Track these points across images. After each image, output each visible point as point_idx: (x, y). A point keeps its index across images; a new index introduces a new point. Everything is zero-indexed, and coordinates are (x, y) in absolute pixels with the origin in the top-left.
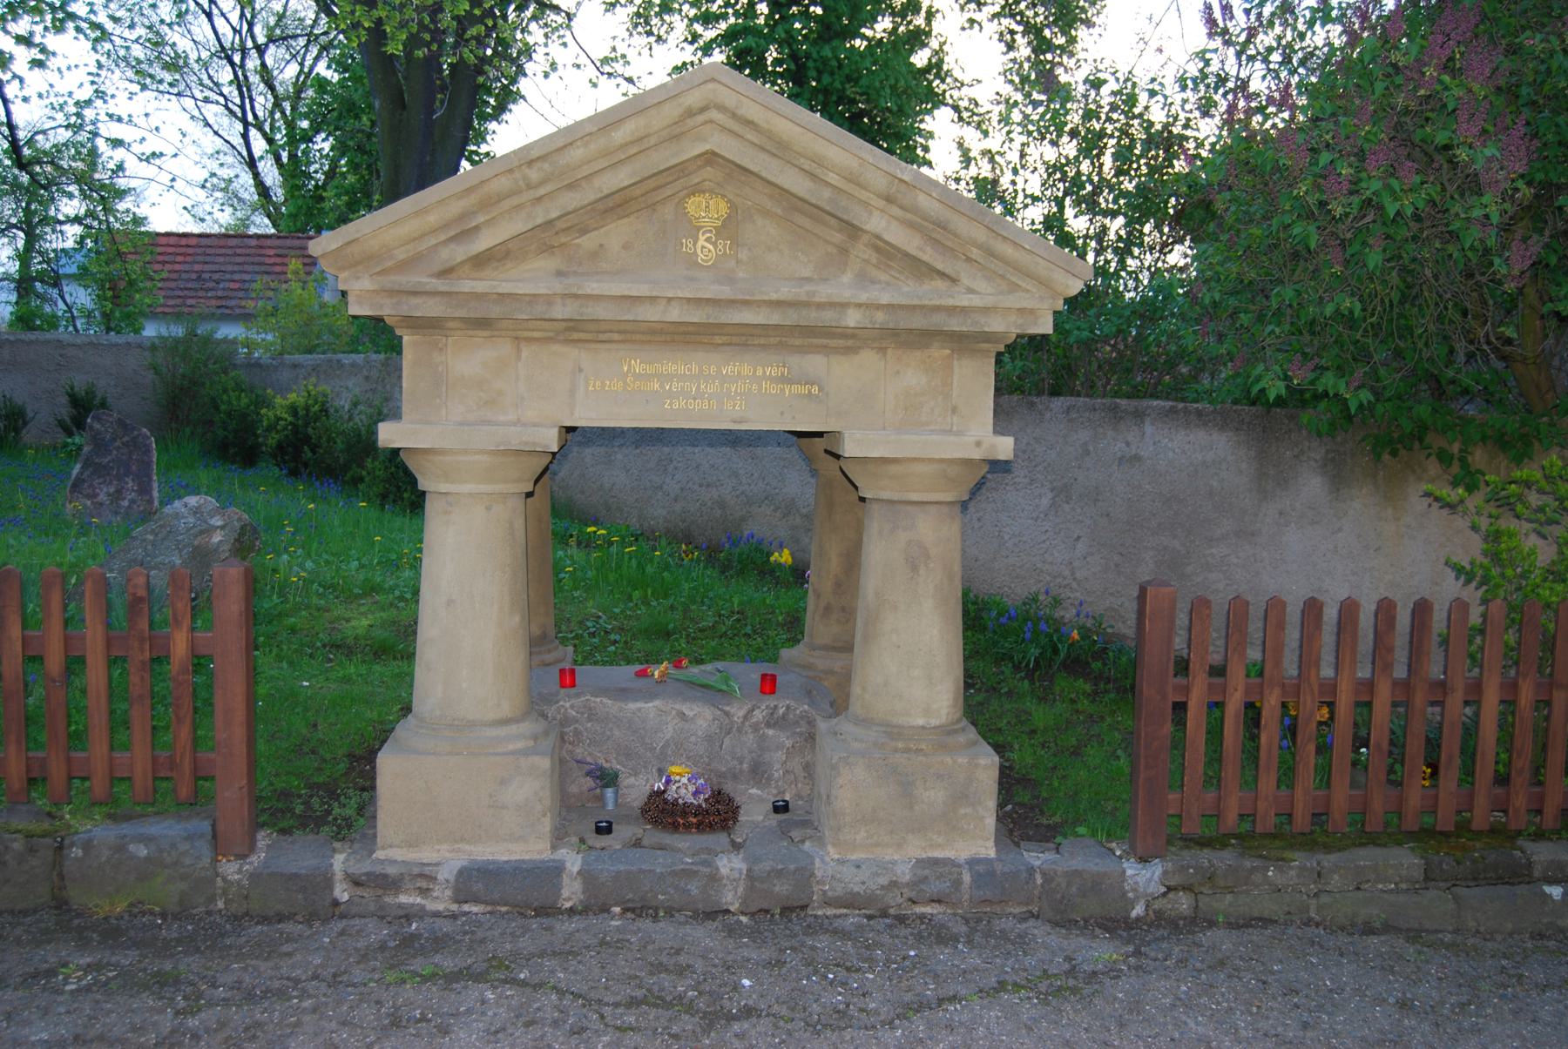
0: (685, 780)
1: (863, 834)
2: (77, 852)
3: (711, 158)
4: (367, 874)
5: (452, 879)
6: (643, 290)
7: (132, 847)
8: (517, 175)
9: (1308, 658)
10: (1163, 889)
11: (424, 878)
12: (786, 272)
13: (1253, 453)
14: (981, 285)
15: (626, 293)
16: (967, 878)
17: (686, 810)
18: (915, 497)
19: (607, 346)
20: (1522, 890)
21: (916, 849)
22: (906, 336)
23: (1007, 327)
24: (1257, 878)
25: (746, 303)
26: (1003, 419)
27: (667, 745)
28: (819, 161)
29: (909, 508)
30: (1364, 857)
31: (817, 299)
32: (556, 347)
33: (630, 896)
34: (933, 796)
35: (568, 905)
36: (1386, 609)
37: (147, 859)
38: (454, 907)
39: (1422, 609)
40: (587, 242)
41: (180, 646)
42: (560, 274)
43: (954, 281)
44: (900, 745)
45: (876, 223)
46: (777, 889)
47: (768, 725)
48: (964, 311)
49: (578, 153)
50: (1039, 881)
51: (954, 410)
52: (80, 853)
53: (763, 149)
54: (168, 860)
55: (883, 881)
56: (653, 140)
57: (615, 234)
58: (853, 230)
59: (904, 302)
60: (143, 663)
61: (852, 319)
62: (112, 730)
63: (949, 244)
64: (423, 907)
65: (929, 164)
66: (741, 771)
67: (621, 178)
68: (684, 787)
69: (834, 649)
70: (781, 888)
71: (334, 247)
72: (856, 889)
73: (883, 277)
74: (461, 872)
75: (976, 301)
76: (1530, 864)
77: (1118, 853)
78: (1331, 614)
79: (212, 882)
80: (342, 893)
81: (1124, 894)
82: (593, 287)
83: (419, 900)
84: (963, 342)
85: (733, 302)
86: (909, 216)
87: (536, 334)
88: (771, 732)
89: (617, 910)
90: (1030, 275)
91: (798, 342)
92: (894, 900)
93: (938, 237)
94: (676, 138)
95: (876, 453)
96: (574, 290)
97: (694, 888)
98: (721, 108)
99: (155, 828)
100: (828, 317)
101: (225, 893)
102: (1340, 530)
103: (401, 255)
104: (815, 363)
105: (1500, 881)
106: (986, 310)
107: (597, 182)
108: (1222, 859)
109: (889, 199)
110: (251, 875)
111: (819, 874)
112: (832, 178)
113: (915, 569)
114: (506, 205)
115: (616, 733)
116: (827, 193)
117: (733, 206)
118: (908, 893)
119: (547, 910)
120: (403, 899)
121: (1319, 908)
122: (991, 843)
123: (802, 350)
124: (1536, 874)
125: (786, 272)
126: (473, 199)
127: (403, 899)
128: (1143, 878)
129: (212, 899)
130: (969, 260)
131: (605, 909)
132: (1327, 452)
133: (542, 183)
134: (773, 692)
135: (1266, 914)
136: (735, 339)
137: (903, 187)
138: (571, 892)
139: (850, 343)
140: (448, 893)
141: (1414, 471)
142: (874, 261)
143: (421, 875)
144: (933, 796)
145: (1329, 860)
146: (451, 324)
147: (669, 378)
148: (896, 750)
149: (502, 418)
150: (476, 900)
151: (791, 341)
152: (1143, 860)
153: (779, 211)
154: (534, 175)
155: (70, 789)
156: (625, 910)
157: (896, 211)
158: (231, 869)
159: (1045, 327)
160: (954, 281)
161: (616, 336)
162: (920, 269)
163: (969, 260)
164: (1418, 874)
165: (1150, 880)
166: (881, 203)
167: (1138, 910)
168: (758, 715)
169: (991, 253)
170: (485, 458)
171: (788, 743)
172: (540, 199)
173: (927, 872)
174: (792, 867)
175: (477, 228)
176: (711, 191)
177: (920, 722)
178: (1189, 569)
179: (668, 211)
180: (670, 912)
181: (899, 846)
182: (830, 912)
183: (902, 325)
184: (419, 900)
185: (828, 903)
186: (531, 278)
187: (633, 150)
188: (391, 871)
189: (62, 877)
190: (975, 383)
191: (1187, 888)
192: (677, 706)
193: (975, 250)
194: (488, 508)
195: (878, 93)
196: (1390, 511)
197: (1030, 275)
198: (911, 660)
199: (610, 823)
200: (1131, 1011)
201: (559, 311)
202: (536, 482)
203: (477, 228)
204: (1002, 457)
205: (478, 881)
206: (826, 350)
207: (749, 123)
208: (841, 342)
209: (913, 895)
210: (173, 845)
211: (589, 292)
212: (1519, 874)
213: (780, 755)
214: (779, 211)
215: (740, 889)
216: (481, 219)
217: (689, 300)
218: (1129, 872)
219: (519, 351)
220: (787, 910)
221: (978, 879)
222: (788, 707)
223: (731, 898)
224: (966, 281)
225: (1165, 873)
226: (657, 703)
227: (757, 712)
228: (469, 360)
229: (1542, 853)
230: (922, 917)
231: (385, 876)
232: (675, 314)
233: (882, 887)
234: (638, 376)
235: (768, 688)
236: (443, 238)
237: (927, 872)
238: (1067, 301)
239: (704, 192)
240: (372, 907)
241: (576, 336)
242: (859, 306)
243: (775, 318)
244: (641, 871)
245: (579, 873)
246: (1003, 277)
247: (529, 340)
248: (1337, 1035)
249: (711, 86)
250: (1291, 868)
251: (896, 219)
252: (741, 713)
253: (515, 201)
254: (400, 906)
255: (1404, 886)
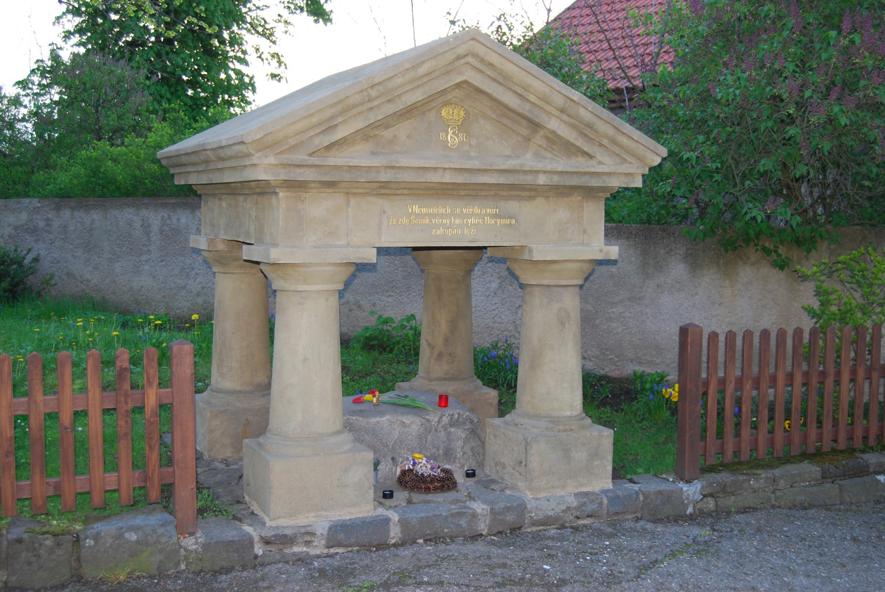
0: (424, 462)
1: (544, 482)
2: (89, 542)
3: (463, 85)
4: (273, 536)
5: (325, 533)
6: (432, 164)
7: (127, 535)
8: (365, 93)
9: (763, 364)
10: (701, 497)
11: (308, 535)
12: (501, 154)
13: (639, 252)
14: (606, 159)
15: (422, 166)
16: (605, 501)
17: (433, 479)
18: (563, 282)
19: (399, 197)
20: (867, 478)
21: (572, 488)
22: (562, 191)
23: (616, 183)
24: (745, 485)
25: (486, 171)
26: (610, 234)
27: (395, 443)
28: (526, 88)
29: (559, 289)
30: (792, 469)
31: (525, 169)
32: (370, 199)
33: (428, 532)
34: (580, 455)
35: (393, 541)
36: (781, 334)
37: (138, 542)
38: (326, 551)
39: (798, 332)
40: (387, 134)
41: (152, 398)
42: (373, 153)
43: (591, 157)
44: (561, 428)
45: (553, 124)
46: (508, 518)
47: (451, 426)
48: (598, 174)
49: (399, 81)
50: (642, 499)
51: (584, 232)
52: (92, 542)
53: (494, 80)
54: (151, 541)
55: (563, 507)
56: (437, 73)
57: (402, 130)
58: (535, 126)
59: (570, 170)
60: (127, 411)
61: (542, 180)
62: (706, 414)
63: (592, 136)
64: (307, 553)
65: (247, 64)
66: (439, 455)
67: (417, 96)
68: (424, 467)
69: (445, 379)
70: (510, 518)
71: (258, 137)
72: (549, 514)
73: (549, 155)
74: (330, 528)
75: (605, 169)
76: (867, 466)
77: (671, 480)
78: (773, 336)
79: (178, 552)
80: (259, 550)
81: (683, 502)
82: (404, 162)
83: (305, 549)
84: (589, 192)
85: (479, 170)
86: (572, 120)
87: (360, 191)
88: (453, 430)
89: (421, 541)
90: (633, 155)
91: (505, 194)
92: (569, 517)
93: (586, 132)
94: (448, 73)
95: (549, 258)
96: (394, 164)
97: (463, 522)
98: (475, 55)
99: (139, 520)
100: (528, 179)
101: (186, 558)
102: (697, 294)
103: (292, 142)
104: (513, 206)
105: (856, 475)
106: (609, 174)
107: (404, 98)
108: (724, 477)
109: (562, 111)
110: (204, 545)
111: (529, 506)
112: (532, 98)
113: (563, 324)
114: (355, 111)
115: (367, 437)
116: (528, 106)
117: (467, 113)
118: (575, 513)
119: (382, 546)
120: (296, 549)
121: (776, 499)
122: (610, 480)
123: (507, 198)
124: (871, 470)
125: (501, 154)
126: (339, 108)
127: (296, 549)
128: (692, 490)
129: (178, 564)
130: (601, 145)
131: (414, 542)
132: (687, 250)
133: (377, 97)
134: (446, 406)
135: (752, 505)
136: (471, 193)
137: (572, 104)
138: (395, 533)
139: (532, 193)
140: (323, 542)
141: (742, 259)
142: (545, 146)
143: (307, 533)
144: (580, 455)
145: (777, 472)
146: (313, 185)
147: (434, 216)
148: (559, 431)
149: (338, 243)
150: (339, 545)
151: (502, 193)
152: (688, 482)
153: (494, 116)
154: (373, 93)
155: (76, 500)
156: (426, 541)
157: (565, 118)
158: (190, 543)
159: (638, 183)
160: (591, 157)
161: (406, 192)
162: (570, 149)
163: (601, 145)
164: (818, 475)
165: (695, 492)
166: (557, 113)
167: (690, 510)
168: (445, 420)
169: (614, 142)
170: (331, 268)
171: (463, 436)
172: (371, 109)
173: (585, 500)
174: (515, 504)
175: (336, 126)
176: (456, 104)
177: (568, 414)
178: (597, 322)
179: (432, 116)
180: (453, 539)
181: (563, 487)
182: (534, 529)
183: (567, 183)
184: (305, 549)
185: (534, 524)
186: (359, 156)
187: (425, 80)
188: (288, 532)
189: (78, 559)
190: (594, 216)
191: (711, 495)
192: (400, 418)
193: (605, 140)
194: (327, 300)
195: (213, 14)
196: (728, 282)
197: (633, 155)
198: (554, 381)
199: (392, 492)
200: (741, 558)
201: (384, 177)
202: (586, 279)
203: (336, 126)
204: (613, 258)
205: (341, 533)
206: (519, 198)
207: (491, 65)
208: (527, 193)
209: (578, 514)
210: (154, 531)
211: (402, 165)
212: (862, 471)
213: (460, 443)
214: (494, 116)
215: (488, 521)
216: (340, 120)
217: (455, 169)
218: (685, 489)
219: (348, 201)
220: (513, 530)
221: (611, 501)
222: (459, 414)
223: (483, 527)
224: (599, 157)
225: (702, 487)
226: (388, 417)
227: (444, 418)
228: (319, 206)
229: (872, 459)
230: (585, 526)
231: (286, 536)
232: (448, 178)
233: (563, 511)
234: (418, 216)
235: (443, 404)
236: (318, 131)
237: (585, 500)
238: (651, 169)
239: (451, 104)
240: (278, 557)
241: (383, 191)
242: (545, 172)
243: (502, 180)
244: (435, 516)
245: (399, 521)
246: (618, 155)
247: (355, 194)
248: (838, 557)
249: (472, 42)
250: (762, 478)
251: (564, 122)
252: (436, 419)
253: (360, 109)
254: (294, 554)
255: (813, 483)
